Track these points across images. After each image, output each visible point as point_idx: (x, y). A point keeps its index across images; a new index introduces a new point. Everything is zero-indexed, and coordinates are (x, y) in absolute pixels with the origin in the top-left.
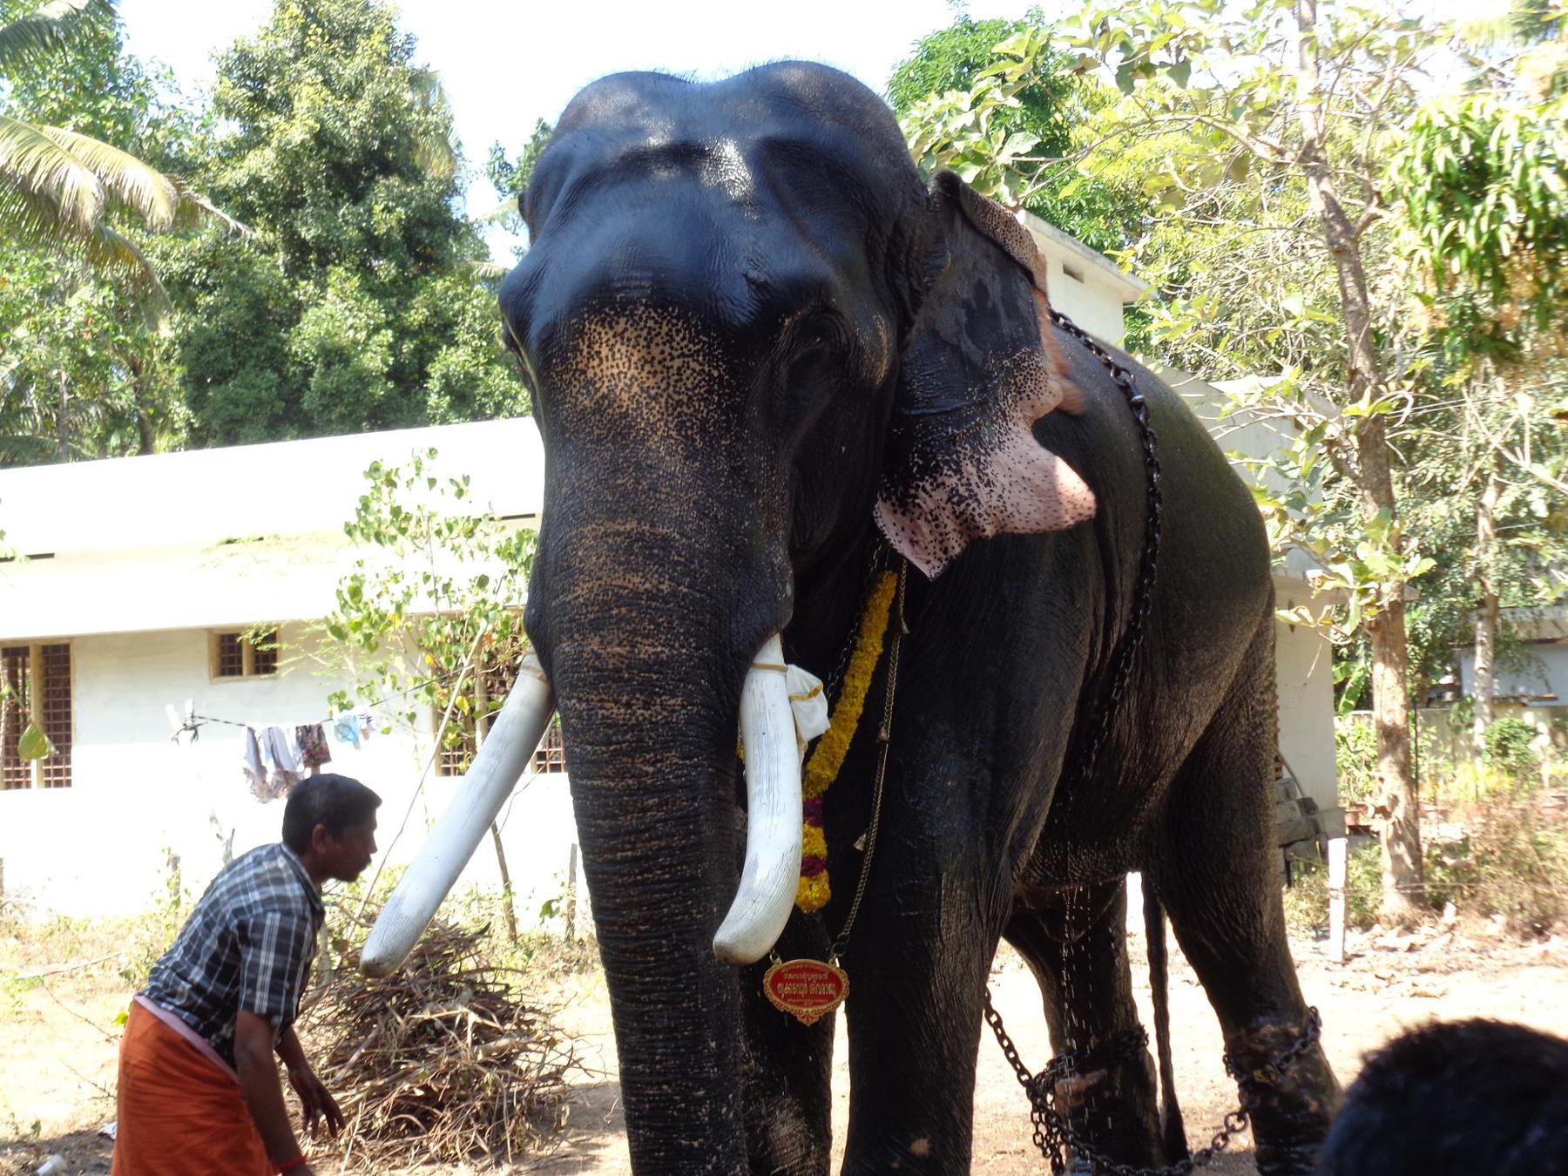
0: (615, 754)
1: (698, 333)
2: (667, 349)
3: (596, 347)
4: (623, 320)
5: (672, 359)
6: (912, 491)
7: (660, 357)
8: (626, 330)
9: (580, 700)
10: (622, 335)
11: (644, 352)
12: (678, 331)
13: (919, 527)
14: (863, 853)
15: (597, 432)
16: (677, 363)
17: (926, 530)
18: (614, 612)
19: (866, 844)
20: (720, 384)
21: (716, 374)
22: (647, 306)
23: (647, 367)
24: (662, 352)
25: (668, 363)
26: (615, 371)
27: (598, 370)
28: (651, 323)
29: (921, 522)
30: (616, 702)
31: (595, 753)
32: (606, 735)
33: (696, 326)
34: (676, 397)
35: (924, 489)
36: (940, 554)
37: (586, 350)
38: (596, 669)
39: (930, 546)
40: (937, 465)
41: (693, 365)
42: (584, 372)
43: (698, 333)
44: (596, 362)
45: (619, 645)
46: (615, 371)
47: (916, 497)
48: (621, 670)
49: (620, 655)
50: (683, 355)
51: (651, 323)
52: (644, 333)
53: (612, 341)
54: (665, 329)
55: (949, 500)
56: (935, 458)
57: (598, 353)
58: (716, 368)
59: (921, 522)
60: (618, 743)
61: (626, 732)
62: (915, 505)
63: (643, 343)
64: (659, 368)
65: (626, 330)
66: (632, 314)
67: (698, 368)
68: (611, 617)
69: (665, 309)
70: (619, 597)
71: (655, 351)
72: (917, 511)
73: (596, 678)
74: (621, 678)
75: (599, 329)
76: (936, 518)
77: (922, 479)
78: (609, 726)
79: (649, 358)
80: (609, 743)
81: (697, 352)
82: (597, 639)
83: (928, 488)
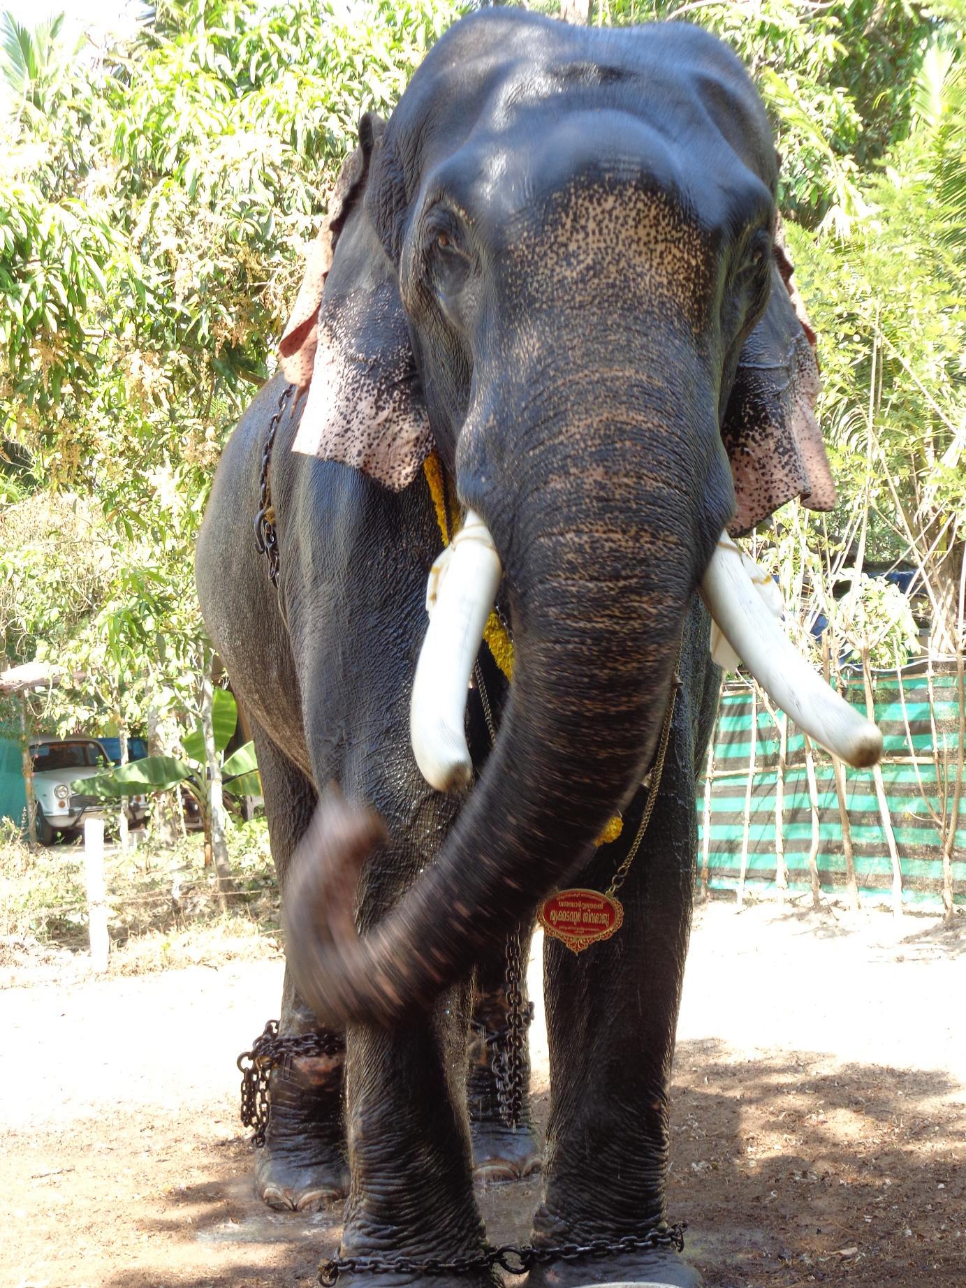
0: (624, 591)
1: (680, 222)
2: (653, 233)
3: (583, 222)
4: (611, 199)
5: (657, 242)
6: (742, 440)
7: (645, 239)
8: (614, 208)
9: (579, 532)
10: (610, 212)
11: (632, 232)
12: (664, 217)
13: (745, 474)
14: (650, 790)
15: (578, 299)
16: (661, 247)
17: (752, 477)
18: (618, 445)
19: (652, 782)
20: (697, 273)
21: (694, 263)
22: (636, 189)
23: (634, 246)
24: (648, 235)
25: (652, 246)
26: (602, 245)
27: (583, 244)
28: (640, 205)
29: (749, 470)
30: (624, 532)
31: (600, 590)
32: (615, 569)
33: (679, 215)
34: (657, 278)
35: (753, 439)
36: (764, 502)
37: (568, 226)
38: (599, 499)
39: (756, 494)
40: (766, 417)
41: (675, 251)
42: (566, 245)
43: (680, 222)
44: (581, 236)
45: (626, 476)
46: (602, 245)
47: (745, 445)
48: (629, 501)
49: (627, 485)
50: (666, 240)
51: (640, 205)
52: (634, 214)
53: (600, 217)
54: (653, 212)
55: (776, 450)
56: (764, 410)
57: (584, 228)
58: (695, 257)
59: (749, 470)
60: (625, 578)
61: (633, 568)
62: (742, 452)
63: (631, 222)
64: (644, 249)
65: (614, 208)
66: (621, 194)
67: (678, 255)
68: (616, 449)
69: (654, 193)
70: (622, 431)
71: (642, 232)
72: (745, 459)
73: (603, 509)
74: (630, 508)
75: (587, 204)
76: (764, 467)
77: (752, 429)
78: (617, 559)
79: (636, 238)
80: (617, 577)
81: (679, 239)
82: (601, 470)
83: (758, 437)
